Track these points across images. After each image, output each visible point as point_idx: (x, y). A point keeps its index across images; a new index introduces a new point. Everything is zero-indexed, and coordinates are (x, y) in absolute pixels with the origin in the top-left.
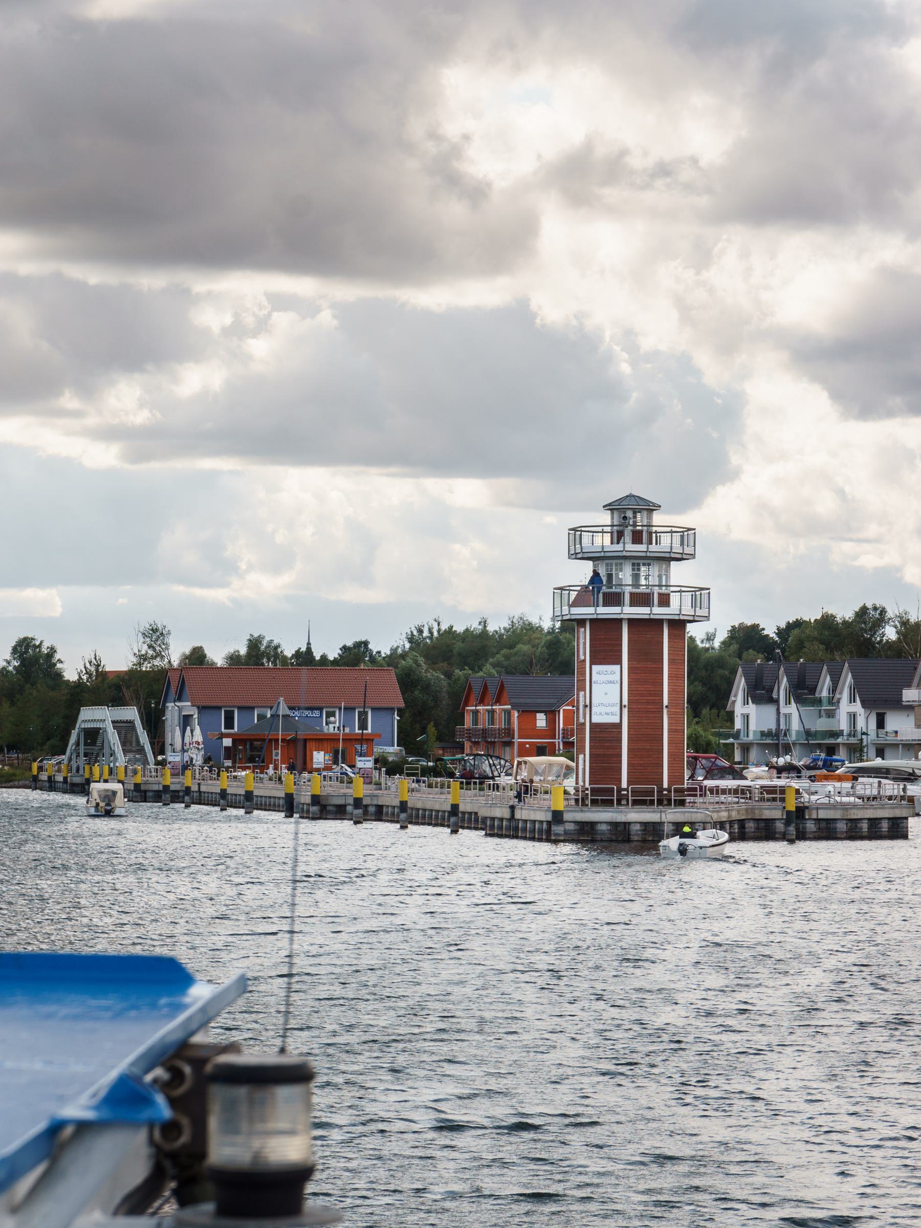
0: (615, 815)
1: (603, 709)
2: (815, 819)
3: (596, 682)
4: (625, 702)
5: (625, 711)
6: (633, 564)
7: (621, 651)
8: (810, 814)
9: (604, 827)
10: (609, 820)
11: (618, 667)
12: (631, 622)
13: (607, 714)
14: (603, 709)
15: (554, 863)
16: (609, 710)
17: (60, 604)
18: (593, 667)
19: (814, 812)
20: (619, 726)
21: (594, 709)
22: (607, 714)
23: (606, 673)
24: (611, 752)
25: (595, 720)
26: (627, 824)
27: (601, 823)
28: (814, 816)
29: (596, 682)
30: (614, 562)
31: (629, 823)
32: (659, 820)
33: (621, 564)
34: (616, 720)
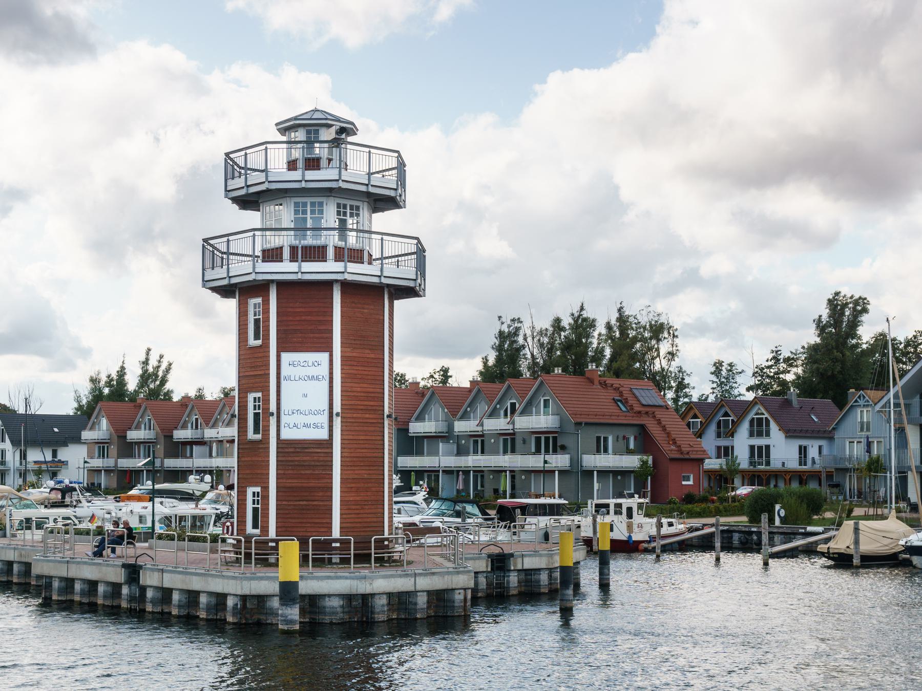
0: (355, 583)
1: (300, 419)
2: (519, 570)
3: (288, 378)
4: (337, 408)
5: (337, 422)
6: (339, 206)
7: (331, 331)
8: (515, 565)
9: (336, 603)
10: (388, 590)
11: (326, 355)
12: (282, 285)
13: (306, 426)
14: (300, 419)
15: (109, 676)
16: (311, 419)
17: (608, 356)
18: (284, 356)
19: (520, 560)
20: (328, 444)
21: (284, 419)
22: (306, 426)
23: (305, 364)
24: (313, 483)
25: (286, 434)
26: (366, 599)
27: (330, 596)
28: (519, 567)
29: (288, 378)
30: (308, 200)
31: (373, 595)
32: (412, 589)
33: (321, 204)
34: (323, 434)
